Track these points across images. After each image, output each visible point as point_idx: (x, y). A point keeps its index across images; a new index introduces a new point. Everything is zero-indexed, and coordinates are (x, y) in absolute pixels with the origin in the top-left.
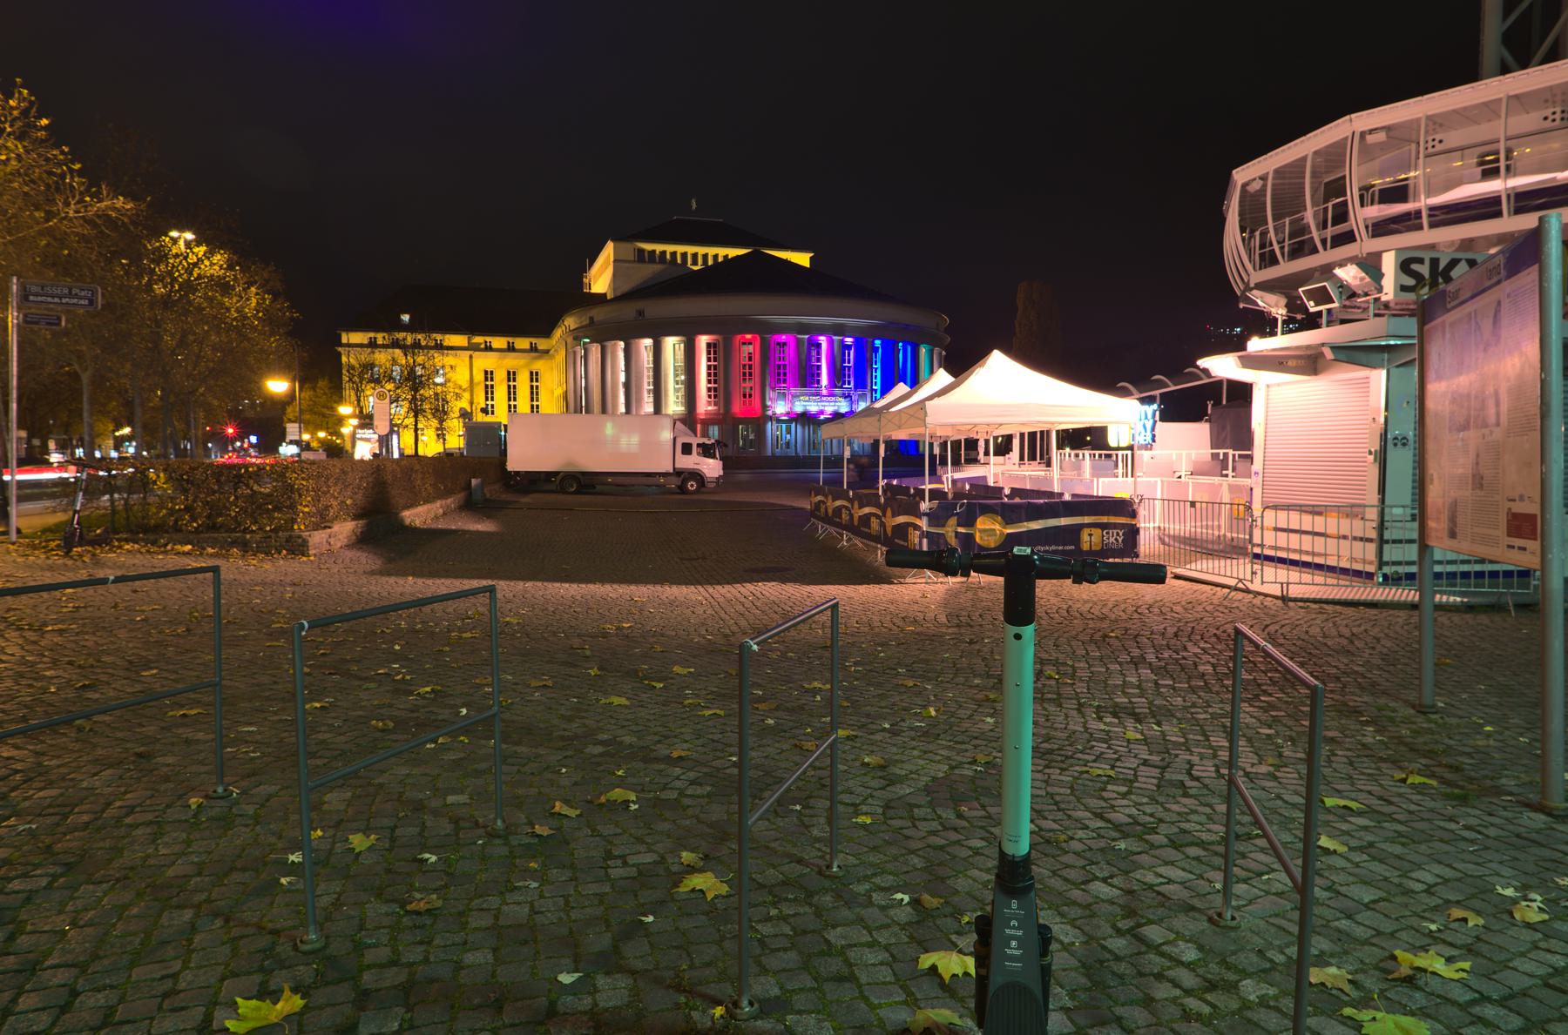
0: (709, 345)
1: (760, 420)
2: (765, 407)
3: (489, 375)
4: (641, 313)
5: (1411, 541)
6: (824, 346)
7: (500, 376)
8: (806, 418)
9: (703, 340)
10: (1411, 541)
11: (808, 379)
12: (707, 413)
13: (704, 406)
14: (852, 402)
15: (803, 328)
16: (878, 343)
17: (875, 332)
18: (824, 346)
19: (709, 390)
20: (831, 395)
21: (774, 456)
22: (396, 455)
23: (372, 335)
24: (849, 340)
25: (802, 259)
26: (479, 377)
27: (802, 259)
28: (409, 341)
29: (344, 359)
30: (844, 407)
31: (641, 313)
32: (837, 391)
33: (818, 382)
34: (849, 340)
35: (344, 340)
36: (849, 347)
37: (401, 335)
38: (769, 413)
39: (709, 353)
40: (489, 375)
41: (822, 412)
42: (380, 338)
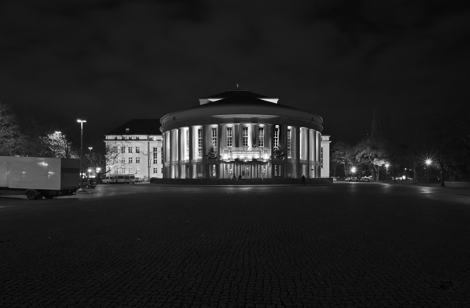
0: (199, 130)
1: (218, 161)
2: (220, 157)
3: (155, 149)
5: (149, 143)
7: (159, 149)
8: (238, 162)
9: (197, 128)
10: (149, 143)
11: (239, 142)
12: (198, 159)
13: (197, 156)
14: (260, 154)
16: (277, 126)
17: (273, 122)
19: (200, 150)
20: (253, 151)
21: (223, 179)
22: (149, 183)
23: (116, 136)
24: (262, 125)
25: (275, 101)
26: (152, 150)
27: (275, 101)
28: (128, 138)
29: (106, 144)
30: (257, 156)
31: (174, 118)
32: (257, 149)
33: (247, 145)
34: (262, 125)
35: (106, 138)
36: (262, 129)
37: (125, 136)
38: (221, 159)
39: (199, 134)
40: (155, 149)
41: (246, 158)
42: (119, 137)
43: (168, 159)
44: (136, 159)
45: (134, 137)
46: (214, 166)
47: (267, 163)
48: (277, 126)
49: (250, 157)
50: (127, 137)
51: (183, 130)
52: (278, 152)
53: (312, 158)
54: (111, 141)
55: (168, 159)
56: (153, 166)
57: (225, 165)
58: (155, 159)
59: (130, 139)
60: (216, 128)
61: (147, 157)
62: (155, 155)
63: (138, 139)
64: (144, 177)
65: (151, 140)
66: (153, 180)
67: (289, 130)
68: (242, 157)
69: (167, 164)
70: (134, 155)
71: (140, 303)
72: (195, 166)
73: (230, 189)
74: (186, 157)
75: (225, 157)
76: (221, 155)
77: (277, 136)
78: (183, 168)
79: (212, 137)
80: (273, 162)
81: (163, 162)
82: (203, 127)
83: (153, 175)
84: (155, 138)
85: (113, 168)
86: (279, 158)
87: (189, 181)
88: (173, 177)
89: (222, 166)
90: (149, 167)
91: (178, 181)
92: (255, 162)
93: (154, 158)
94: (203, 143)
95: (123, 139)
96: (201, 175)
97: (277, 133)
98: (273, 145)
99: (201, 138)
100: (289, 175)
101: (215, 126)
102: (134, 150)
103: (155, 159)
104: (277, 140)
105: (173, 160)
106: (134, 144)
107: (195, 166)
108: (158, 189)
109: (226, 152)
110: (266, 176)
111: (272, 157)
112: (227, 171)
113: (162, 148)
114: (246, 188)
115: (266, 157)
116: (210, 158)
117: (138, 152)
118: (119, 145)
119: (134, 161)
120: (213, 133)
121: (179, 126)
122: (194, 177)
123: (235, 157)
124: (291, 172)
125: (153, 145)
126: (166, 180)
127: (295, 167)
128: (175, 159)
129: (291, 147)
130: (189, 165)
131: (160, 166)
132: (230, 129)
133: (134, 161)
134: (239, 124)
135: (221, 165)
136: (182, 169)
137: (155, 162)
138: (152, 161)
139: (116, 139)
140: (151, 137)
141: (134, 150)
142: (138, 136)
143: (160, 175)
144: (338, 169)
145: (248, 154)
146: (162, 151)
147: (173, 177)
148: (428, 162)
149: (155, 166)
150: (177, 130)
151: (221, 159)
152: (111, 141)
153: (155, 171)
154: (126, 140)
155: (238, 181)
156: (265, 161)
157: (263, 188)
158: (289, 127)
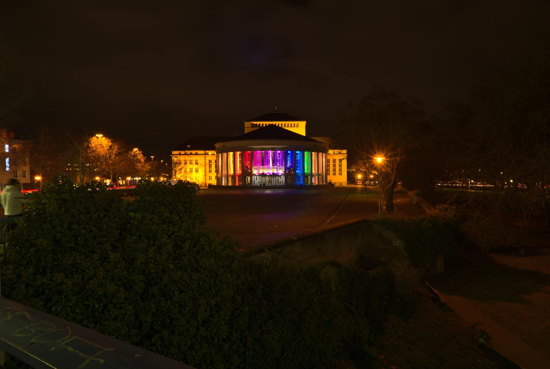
1: (251, 175)
3: (210, 161)
4: (224, 146)
6: (271, 154)
7: (213, 162)
8: (263, 175)
9: (238, 153)
11: (264, 162)
13: (239, 171)
15: (262, 149)
16: (289, 152)
18: (271, 154)
26: (207, 162)
30: (275, 172)
31: (224, 146)
32: (275, 167)
37: (187, 151)
40: (210, 161)
42: (183, 152)
43: (220, 172)
44: (197, 170)
45: (194, 152)
47: (281, 176)
48: (289, 152)
49: (271, 172)
50: (189, 152)
52: (288, 169)
53: (320, 172)
54: (177, 156)
55: (220, 172)
56: (209, 174)
59: (191, 154)
61: (203, 168)
62: (210, 166)
63: (197, 154)
65: (207, 154)
66: (210, 186)
67: (298, 154)
68: (266, 172)
69: (219, 175)
70: (195, 167)
72: (237, 178)
73: (258, 191)
74: (232, 172)
75: (255, 172)
78: (230, 179)
80: (285, 174)
81: (217, 171)
83: (209, 182)
84: (210, 153)
85: (179, 176)
86: (290, 173)
87: (234, 187)
88: (223, 184)
89: (254, 178)
90: (205, 175)
91: (227, 187)
92: (274, 175)
94: (242, 163)
95: (186, 154)
96: (241, 183)
98: (286, 164)
100: (297, 183)
102: (194, 162)
105: (224, 173)
106: (194, 158)
107: (237, 178)
108: (214, 192)
109: (256, 169)
110: (281, 184)
111: (285, 171)
112: (257, 181)
113: (216, 161)
114: (268, 192)
115: (281, 172)
116: (246, 172)
117: (197, 163)
118: (182, 158)
119: (194, 170)
121: (227, 151)
122: (237, 184)
123: (261, 172)
124: (299, 181)
125: (208, 158)
126: (219, 186)
127: (301, 177)
128: (225, 172)
129: (300, 164)
130: (234, 177)
131: (214, 175)
133: (194, 170)
135: (253, 177)
136: (308, 168)
137: (210, 171)
138: (208, 171)
139: (180, 154)
140: (207, 152)
141: (194, 162)
142: (197, 151)
143: (214, 182)
144: (351, 178)
145: (270, 170)
146: (216, 162)
147: (223, 184)
149: (210, 174)
152: (177, 156)
153: (210, 178)
154: (188, 155)
155: (263, 186)
157: (280, 191)
158: (298, 152)
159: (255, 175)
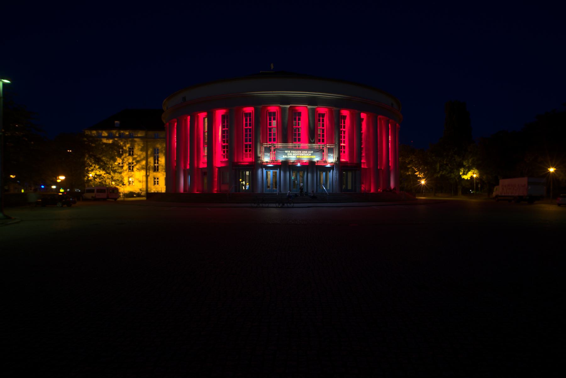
0: (223, 117)
1: (256, 165)
2: (257, 158)
9: (220, 113)
11: (288, 136)
19: (224, 147)
37: (114, 131)
38: (259, 162)
39: (223, 122)
46: (247, 173)
51: (198, 117)
57: (265, 171)
58: (156, 165)
60: (250, 114)
64: (140, 190)
66: (149, 195)
67: (344, 117)
71: (138, 159)
73: (273, 211)
75: (266, 159)
76: (259, 155)
77: (344, 128)
79: (244, 127)
82: (255, 109)
83: (153, 189)
92: (311, 166)
93: (155, 163)
97: (344, 123)
99: (226, 129)
101: (249, 110)
103: (156, 165)
104: (344, 133)
109: (268, 150)
111: (339, 158)
120: (246, 120)
131: (161, 176)
132: (247, 115)
134: (288, 106)
135: (260, 171)
143: (161, 187)
148: (552, 170)
150: (189, 118)
151: (259, 162)
153: (156, 182)
156: (328, 166)
159: (264, 166)
